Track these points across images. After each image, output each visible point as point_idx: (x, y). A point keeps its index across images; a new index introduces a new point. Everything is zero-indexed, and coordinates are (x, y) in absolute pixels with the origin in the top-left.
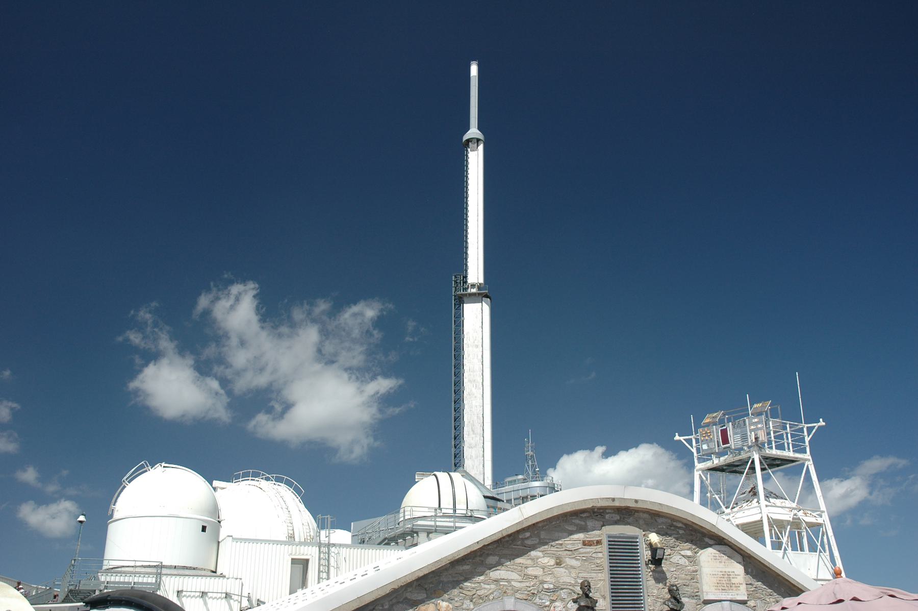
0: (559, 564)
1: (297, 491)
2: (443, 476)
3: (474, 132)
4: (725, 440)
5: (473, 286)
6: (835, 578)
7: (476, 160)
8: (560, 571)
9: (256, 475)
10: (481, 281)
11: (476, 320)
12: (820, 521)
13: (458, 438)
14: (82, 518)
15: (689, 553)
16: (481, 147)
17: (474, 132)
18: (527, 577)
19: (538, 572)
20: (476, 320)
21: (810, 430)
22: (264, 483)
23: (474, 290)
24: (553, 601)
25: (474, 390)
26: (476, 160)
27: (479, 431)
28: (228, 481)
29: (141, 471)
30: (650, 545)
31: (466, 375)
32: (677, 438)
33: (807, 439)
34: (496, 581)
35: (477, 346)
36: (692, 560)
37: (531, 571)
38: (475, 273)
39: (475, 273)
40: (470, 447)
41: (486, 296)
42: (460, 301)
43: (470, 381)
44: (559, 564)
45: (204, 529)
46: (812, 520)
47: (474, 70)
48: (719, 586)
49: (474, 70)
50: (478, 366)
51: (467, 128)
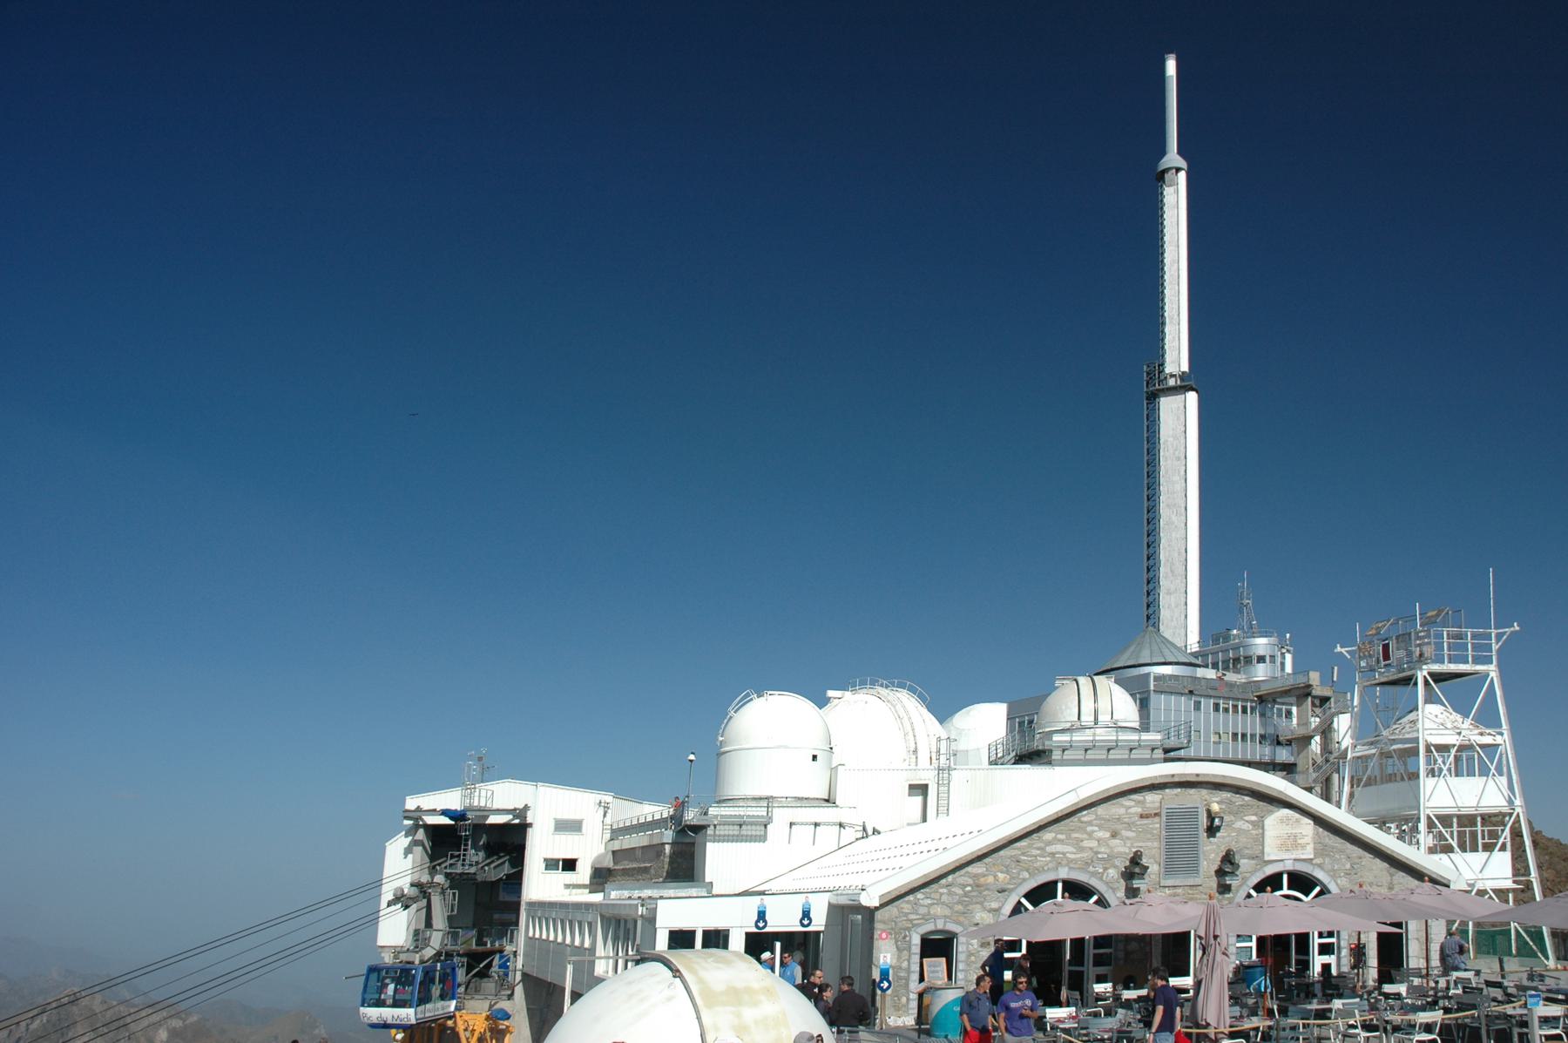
0: (1114, 835)
1: (922, 698)
2: (1083, 680)
3: (1173, 158)
4: (1386, 656)
5: (1172, 376)
6: (1221, 893)
7: (1176, 200)
8: (1116, 842)
9: (873, 683)
10: (1185, 367)
11: (1180, 421)
12: (1499, 740)
13: (1152, 581)
14: (692, 757)
15: (1254, 818)
16: (1182, 176)
17: (1173, 158)
18: (1082, 849)
19: (1094, 844)
20: (1180, 421)
21: (1499, 636)
22: (884, 692)
23: (1172, 382)
24: (1105, 869)
25: (1174, 518)
26: (1176, 200)
27: (1180, 569)
28: (844, 689)
29: (746, 700)
30: (1209, 812)
31: (1164, 499)
32: (1339, 649)
33: (1495, 647)
34: (1053, 854)
35: (1178, 459)
36: (1259, 825)
37: (1086, 844)
38: (1177, 356)
39: (1177, 356)
40: (1169, 593)
41: (1192, 389)
42: (1153, 397)
43: (1297, 821)
44: (1114, 835)
45: (815, 757)
46: (1487, 740)
47: (1171, 67)
48: (1283, 847)
49: (1171, 67)
50: (1179, 487)
51: (1162, 152)
